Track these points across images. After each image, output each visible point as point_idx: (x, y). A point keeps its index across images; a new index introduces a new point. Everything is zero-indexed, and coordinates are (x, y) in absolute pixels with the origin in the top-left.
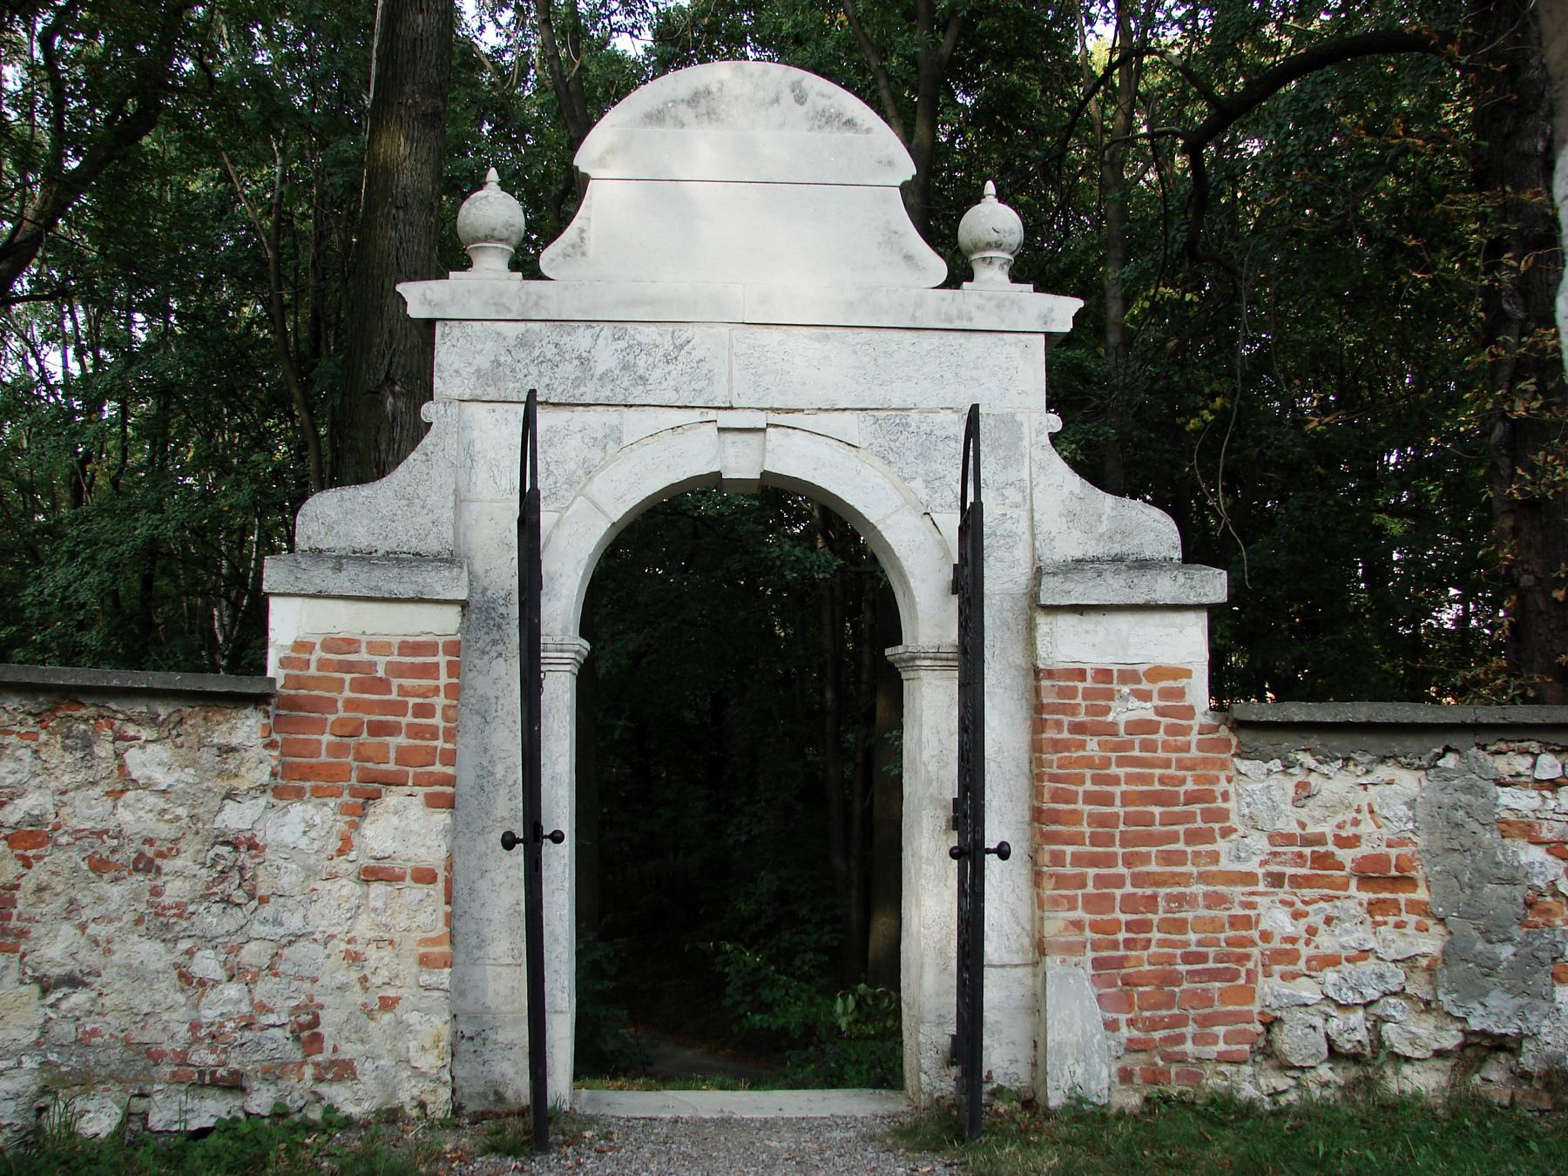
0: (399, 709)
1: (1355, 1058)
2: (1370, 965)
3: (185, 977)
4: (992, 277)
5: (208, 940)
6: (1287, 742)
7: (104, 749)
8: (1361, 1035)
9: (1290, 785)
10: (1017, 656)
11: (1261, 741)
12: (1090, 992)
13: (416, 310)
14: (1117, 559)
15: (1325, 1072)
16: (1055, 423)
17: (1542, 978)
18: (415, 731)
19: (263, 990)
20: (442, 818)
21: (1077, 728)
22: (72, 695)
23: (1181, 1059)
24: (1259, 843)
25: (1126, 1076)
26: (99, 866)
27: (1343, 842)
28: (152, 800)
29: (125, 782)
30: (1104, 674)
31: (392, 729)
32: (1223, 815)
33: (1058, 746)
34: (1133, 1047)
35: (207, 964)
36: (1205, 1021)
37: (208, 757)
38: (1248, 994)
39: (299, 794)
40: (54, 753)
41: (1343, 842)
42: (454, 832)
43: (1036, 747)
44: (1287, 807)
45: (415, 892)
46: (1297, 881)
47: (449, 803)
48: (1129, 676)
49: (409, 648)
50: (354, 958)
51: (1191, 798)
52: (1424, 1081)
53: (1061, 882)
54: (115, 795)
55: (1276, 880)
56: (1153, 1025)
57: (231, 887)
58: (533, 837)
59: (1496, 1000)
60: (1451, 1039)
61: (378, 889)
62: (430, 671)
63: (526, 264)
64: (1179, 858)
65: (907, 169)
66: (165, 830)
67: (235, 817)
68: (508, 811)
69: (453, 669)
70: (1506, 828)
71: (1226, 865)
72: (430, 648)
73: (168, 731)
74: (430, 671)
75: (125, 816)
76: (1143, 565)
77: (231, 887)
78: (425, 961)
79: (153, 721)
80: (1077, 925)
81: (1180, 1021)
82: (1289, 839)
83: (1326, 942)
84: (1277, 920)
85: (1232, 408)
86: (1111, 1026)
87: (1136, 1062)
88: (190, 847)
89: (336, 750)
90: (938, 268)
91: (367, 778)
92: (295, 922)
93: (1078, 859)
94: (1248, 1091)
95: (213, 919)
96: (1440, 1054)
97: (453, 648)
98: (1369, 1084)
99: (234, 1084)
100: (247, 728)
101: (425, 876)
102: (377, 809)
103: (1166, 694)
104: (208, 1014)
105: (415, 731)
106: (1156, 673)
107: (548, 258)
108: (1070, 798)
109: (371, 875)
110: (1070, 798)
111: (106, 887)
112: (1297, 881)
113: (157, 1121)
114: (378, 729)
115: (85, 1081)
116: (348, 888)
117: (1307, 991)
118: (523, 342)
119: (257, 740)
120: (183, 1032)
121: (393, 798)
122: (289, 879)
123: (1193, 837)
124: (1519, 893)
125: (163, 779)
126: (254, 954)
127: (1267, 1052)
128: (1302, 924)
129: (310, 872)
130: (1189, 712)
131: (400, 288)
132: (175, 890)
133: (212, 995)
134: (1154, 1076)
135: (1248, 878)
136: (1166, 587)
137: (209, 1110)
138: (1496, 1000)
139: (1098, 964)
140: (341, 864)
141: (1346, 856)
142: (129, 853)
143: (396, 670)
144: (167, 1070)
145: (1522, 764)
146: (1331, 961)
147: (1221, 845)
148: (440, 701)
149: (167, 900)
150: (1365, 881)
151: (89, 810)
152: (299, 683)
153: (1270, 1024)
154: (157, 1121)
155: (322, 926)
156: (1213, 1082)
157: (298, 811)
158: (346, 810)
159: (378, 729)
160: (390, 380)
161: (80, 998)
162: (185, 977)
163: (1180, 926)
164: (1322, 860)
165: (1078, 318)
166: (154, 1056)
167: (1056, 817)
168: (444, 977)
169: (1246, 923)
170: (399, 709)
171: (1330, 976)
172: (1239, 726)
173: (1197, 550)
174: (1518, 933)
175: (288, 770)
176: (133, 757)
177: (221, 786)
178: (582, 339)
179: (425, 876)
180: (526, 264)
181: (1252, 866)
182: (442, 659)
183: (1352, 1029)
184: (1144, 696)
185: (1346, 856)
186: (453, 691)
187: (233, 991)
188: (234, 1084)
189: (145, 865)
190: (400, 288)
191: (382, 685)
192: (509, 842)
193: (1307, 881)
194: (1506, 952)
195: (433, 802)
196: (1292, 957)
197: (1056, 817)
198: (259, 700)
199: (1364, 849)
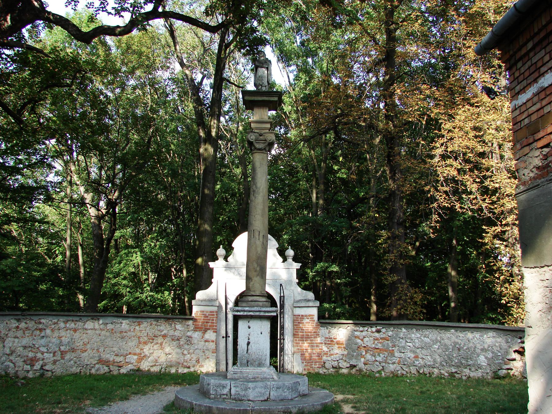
0: (210, 320)
1: (336, 368)
2: (338, 355)
3: (183, 354)
4: (290, 260)
5: (186, 349)
6: (327, 325)
7: (173, 325)
8: (336, 365)
9: (328, 331)
10: (290, 313)
11: (324, 325)
12: (300, 358)
13: (211, 266)
14: (305, 300)
15: (332, 369)
16: (297, 281)
17: (359, 357)
18: (212, 323)
20: (215, 334)
21: (299, 323)
22: (169, 319)
23: (312, 367)
25: (305, 369)
26: (173, 340)
28: (179, 332)
29: (176, 329)
30: (302, 316)
31: (209, 322)
32: (318, 335)
33: (296, 325)
34: (306, 366)
35: (186, 352)
36: (316, 362)
37: (186, 326)
38: (321, 359)
39: (197, 331)
40: (167, 326)
42: (217, 336)
43: (294, 325)
44: (327, 334)
45: (212, 343)
46: (328, 344)
47: (216, 332)
48: (306, 316)
49: (211, 312)
50: (204, 352)
52: (345, 371)
53: (297, 343)
54: (174, 331)
56: (309, 363)
57: (188, 342)
58: (227, 336)
59: (354, 360)
60: (348, 365)
61: (207, 343)
62: (214, 315)
63: (226, 259)
64: (313, 340)
65: (277, 246)
66: (180, 335)
67: (189, 334)
68: (223, 333)
69: (216, 315)
70: (356, 337)
72: (213, 312)
73: (181, 323)
74: (214, 315)
75: (176, 333)
76: (309, 301)
77: (188, 342)
78: (213, 352)
79: (179, 322)
80: (299, 349)
81: (312, 362)
82: (327, 338)
84: (325, 349)
85: (277, 314)
86: (303, 363)
87: (306, 368)
88: (183, 338)
89: (201, 325)
90: (281, 259)
91: (205, 329)
92: (196, 347)
93: (299, 340)
94: (321, 372)
95: (186, 346)
96: (347, 367)
97: (216, 312)
98: (337, 372)
99: (189, 367)
100: (190, 322)
101: (213, 341)
102: (206, 333)
103: (311, 318)
104: (186, 358)
105: (212, 323)
106: (310, 315)
107: (229, 259)
108: (298, 332)
109: (206, 341)
110: (298, 332)
111: (173, 342)
112: (328, 344)
113: (180, 371)
114: (207, 322)
115: (171, 366)
116: (203, 343)
117: (329, 359)
119: (192, 324)
120: (183, 361)
121: (209, 331)
122: (196, 342)
124: (357, 346)
125: (180, 329)
126: (191, 351)
127: (323, 366)
129: (198, 341)
130: (314, 321)
131: (209, 263)
132: (182, 343)
134: (308, 370)
136: (311, 304)
137: (186, 371)
138: (354, 360)
139: (301, 354)
140: (202, 340)
142: (176, 338)
143: (209, 315)
144: (181, 365)
148: (215, 319)
150: (337, 344)
151: (171, 333)
152: (197, 316)
153: (324, 363)
154: (180, 371)
155: (200, 348)
156: (316, 371)
157: (197, 333)
158: (203, 333)
159: (207, 322)
160: (204, 253)
161: (170, 356)
162: (183, 354)
165: (301, 266)
166: (179, 363)
167: (296, 335)
168: (215, 354)
169: (321, 349)
170: (210, 320)
171: (332, 357)
172: (320, 323)
173: (317, 298)
174: (357, 351)
175: (195, 328)
176: (177, 326)
179: (213, 341)
180: (226, 259)
182: (215, 313)
183: (335, 364)
184: (308, 318)
185: (334, 340)
186: (216, 317)
187: (189, 356)
188: (189, 367)
189: (178, 340)
190: (209, 263)
191: (207, 317)
192: (223, 337)
194: (355, 354)
195: (214, 332)
196: (327, 354)
197: (296, 335)
198: (192, 319)
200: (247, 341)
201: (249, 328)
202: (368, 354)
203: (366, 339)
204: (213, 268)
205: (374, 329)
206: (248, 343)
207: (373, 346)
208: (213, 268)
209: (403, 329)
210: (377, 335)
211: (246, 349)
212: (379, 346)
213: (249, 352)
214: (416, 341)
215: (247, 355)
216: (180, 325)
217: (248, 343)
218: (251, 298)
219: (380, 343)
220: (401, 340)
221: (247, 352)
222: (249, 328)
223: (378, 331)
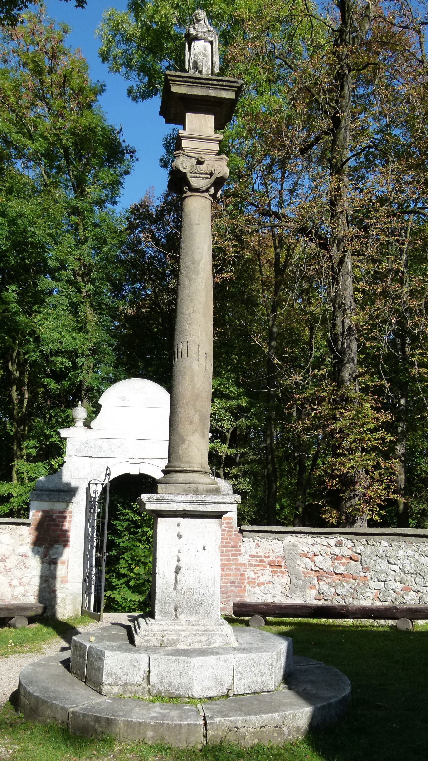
19: (27, 587)
24: (247, 557)
27: (265, 557)
32: (239, 550)
35: (15, 582)
37: (17, 537)
41: (265, 557)
44: (253, 549)
46: (255, 566)
51: (232, 547)
55: (251, 565)
63: (87, 424)
71: (240, 561)
82: (254, 556)
83: (262, 580)
95: (18, 573)
104: (15, 593)
118: (87, 443)
123: (233, 555)
128: (257, 575)
130: (232, 527)
133: (16, 589)
135: (244, 565)
141: (266, 560)
145: (305, 540)
146: (263, 584)
147: (239, 557)
149: (7, 568)
163: (230, 575)
164: (261, 561)
169: (242, 575)
177: (20, 543)
178: (99, 442)
181: (246, 562)
185: (266, 560)
193: (259, 566)
194: (300, 582)
196: (254, 583)
199: (270, 559)
200: (174, 564)
201: (180, 536)
202: (322, 583)
203: (319, 558)
204: (101, 406)
205: (332, 541)
206: (178, 570)
207: (332, 569)
208: (101, 406)
209: (383, 542)
210: (337, 551)
211: (174, 581)
212: (341, 569)
213: (179, 587)
214: (407, 562)
215: (174, 594)
216: (7, 535)
217: (178, 570)
218: (181, 477)
219: (343, 564)
220: (379, 560)
221: (175, 589)
222: (180, 536)
223: (339, 545)
